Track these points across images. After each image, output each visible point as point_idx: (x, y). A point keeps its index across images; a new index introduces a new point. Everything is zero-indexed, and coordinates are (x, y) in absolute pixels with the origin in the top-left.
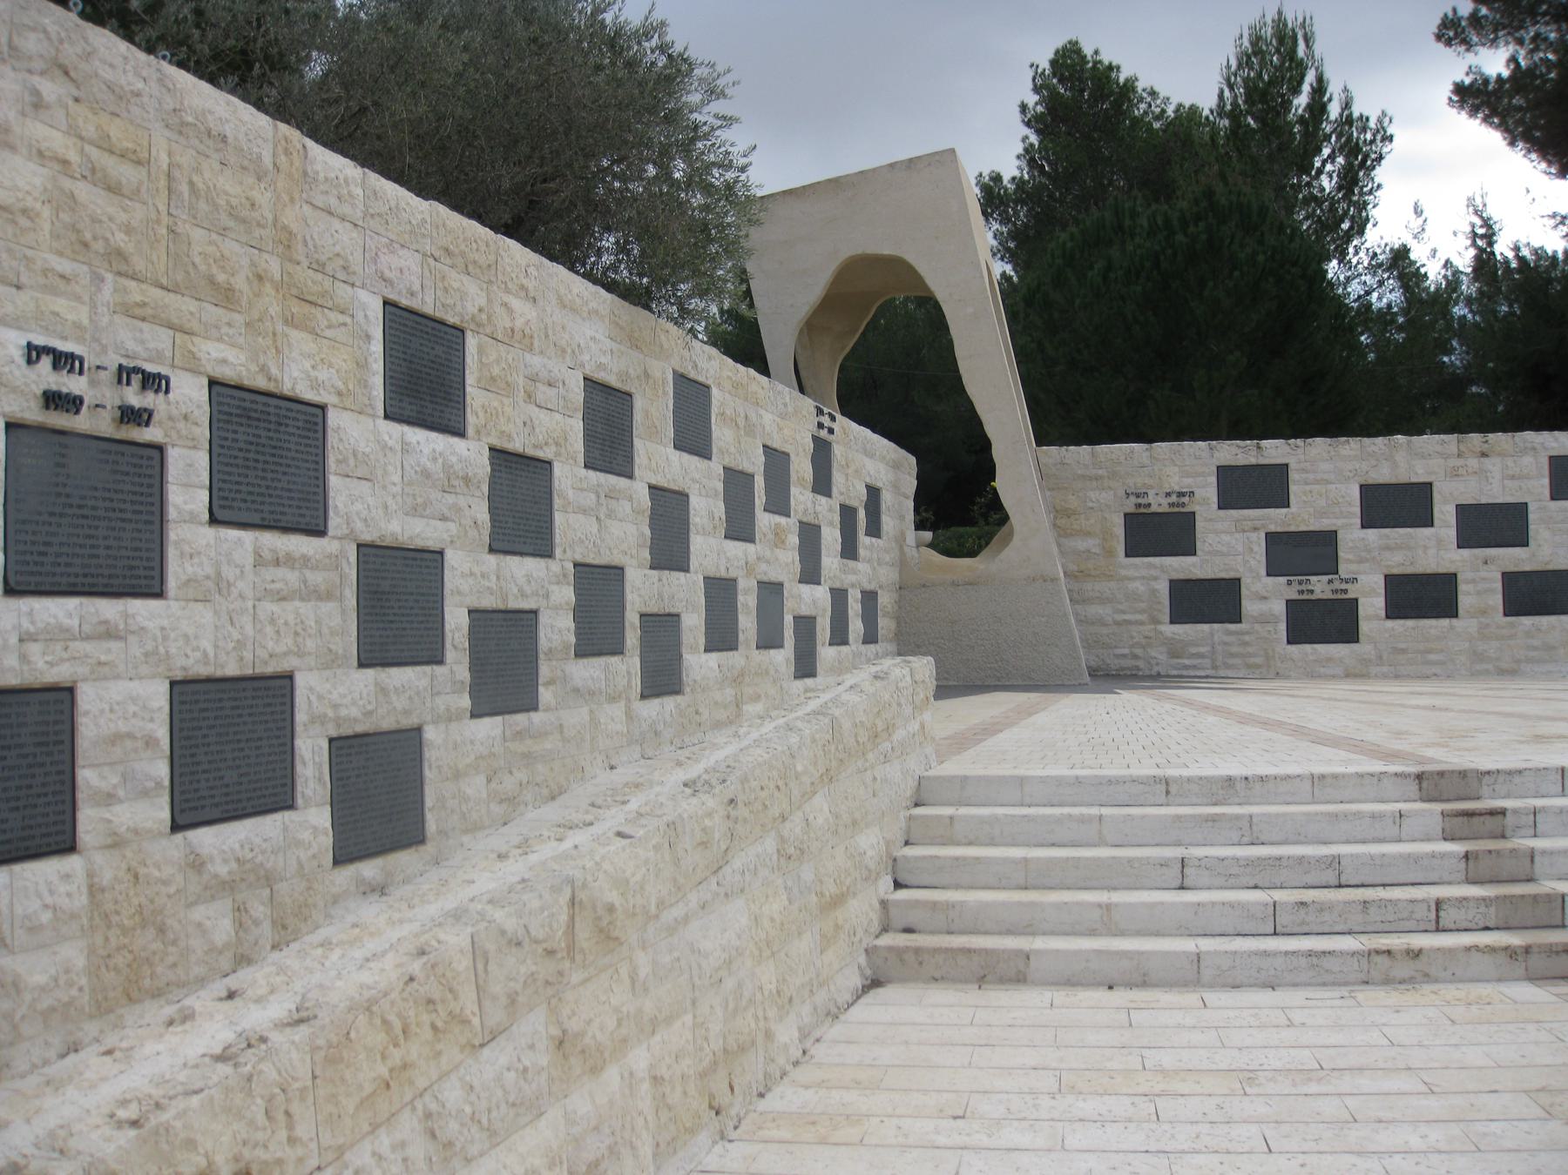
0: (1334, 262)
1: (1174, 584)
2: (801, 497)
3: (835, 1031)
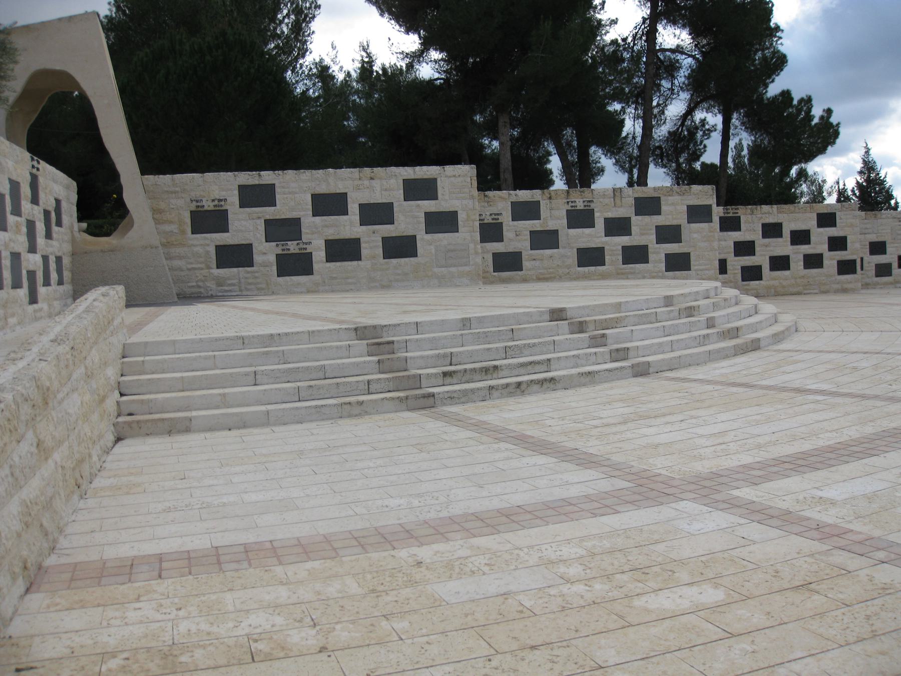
0: (289, 72)
1: (218, 248)
2: (26, 206)
3: (110, 458)
